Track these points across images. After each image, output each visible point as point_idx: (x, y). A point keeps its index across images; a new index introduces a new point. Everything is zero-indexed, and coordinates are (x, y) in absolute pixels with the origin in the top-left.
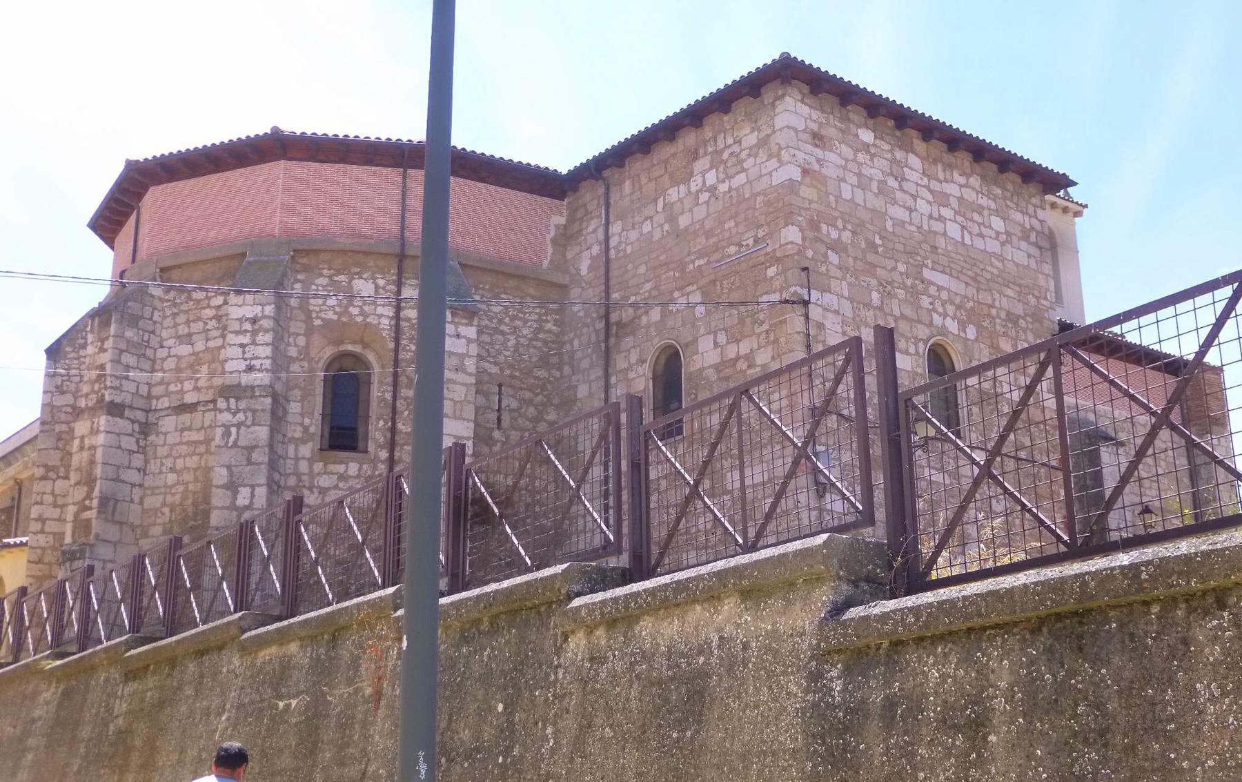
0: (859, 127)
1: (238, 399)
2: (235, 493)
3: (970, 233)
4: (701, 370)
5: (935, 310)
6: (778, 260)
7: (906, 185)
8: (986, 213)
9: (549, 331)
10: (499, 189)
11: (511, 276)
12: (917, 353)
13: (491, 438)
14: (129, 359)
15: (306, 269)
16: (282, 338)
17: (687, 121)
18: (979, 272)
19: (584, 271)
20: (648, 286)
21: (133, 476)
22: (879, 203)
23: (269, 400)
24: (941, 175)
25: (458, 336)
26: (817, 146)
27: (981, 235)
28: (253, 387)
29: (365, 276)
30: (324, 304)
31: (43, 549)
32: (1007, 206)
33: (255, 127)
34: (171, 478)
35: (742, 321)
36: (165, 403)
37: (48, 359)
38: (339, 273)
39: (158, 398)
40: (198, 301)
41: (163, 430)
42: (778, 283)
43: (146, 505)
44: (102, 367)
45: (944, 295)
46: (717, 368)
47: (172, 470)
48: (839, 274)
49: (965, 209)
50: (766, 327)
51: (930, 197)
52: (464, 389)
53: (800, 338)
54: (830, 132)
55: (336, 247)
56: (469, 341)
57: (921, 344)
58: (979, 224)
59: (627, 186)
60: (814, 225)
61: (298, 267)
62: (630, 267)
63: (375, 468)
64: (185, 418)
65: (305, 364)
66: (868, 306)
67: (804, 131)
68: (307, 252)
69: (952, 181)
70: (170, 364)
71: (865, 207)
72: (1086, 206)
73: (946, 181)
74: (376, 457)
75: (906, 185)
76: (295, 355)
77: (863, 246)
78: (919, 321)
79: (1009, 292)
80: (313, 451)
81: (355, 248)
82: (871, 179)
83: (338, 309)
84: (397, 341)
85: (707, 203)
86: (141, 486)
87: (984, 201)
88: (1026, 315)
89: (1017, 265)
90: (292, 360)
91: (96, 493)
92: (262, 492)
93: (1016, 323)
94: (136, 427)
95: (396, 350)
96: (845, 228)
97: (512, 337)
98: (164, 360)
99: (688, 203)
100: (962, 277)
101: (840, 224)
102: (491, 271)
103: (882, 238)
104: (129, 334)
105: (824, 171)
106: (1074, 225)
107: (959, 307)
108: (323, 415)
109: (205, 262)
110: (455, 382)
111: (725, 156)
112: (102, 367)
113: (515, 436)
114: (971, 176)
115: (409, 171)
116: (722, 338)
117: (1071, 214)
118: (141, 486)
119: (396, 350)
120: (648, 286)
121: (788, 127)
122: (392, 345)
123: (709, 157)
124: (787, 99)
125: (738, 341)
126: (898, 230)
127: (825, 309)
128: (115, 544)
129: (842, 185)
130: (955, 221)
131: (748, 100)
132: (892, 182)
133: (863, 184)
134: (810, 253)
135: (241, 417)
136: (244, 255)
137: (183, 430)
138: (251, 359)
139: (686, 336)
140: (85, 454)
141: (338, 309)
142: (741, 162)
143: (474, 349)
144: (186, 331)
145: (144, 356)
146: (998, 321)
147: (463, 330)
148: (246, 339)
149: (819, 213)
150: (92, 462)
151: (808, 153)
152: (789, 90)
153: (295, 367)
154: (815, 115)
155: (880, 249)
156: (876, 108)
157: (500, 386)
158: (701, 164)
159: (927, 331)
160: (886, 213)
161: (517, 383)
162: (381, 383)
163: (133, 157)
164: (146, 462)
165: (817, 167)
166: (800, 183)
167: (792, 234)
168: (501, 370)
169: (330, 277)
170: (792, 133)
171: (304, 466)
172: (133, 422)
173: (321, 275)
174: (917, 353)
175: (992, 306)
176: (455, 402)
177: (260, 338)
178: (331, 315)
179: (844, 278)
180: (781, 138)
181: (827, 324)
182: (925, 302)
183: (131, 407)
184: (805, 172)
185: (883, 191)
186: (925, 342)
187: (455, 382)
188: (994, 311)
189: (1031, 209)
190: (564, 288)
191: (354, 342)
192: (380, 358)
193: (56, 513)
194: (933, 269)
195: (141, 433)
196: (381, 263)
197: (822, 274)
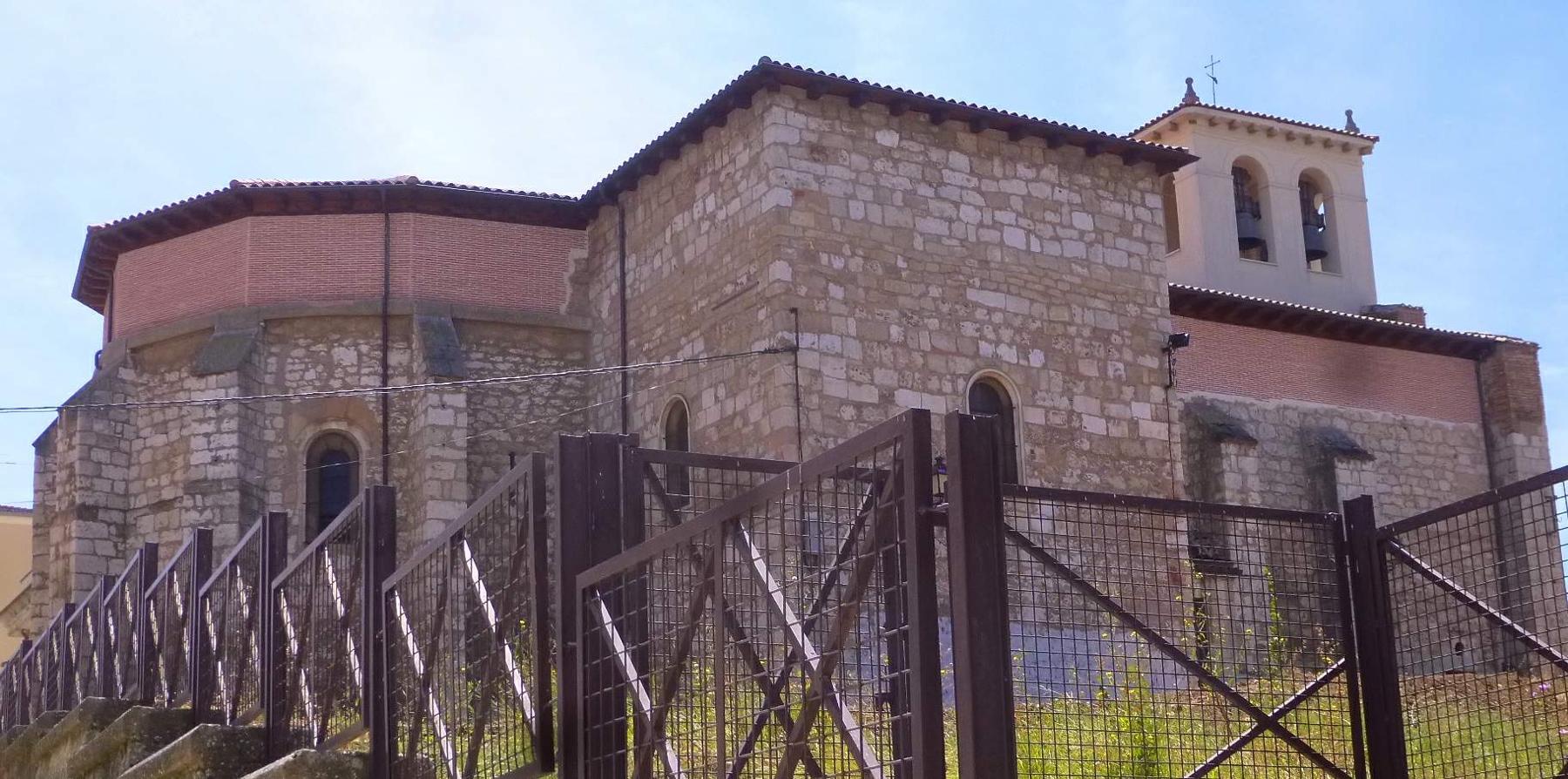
0: (876, 129)
1: (204, 495)
3: (1039, 237)
4: (705, 428)
5: (982, 338)
6: (768, 301)
7: (944, 192)
8: (1065, 210)
9: (571, 386)
10: (503, 224)
11: (518, 326)
12: (955, 392)
14: (100, 455)
15: (281, 340)
16: (254, 423)
17: (683, 139)
18: (1052, 283)
19: (605, 314)
20: (659, 331)
22: (904, 218)
23: (236, 495)
24: (998, 172)
25: (443, 406)
26: (815, 160)
27: (1057, 239)
28: (219, 481)
29: (346, 342)
30: (302, 378)
32: (1099, 197)
33: (214, 182)
35: (738, 371)
36: (143, 501)
37: (37, 453)
38: (316, 341)
39: (136, 496)
40: (173, 383)
41: (142, 531)
42: (768, 329)
45: (998, 318)
46: (718, 426)
48: (843, 309)
49: (1032, 208)
50: (757, 379)
51: (980, 201)
53: (789, 391)
54: (835, 141)
55: (310, 312)
56: (457, 410)
57: (961, 382)
58: (1054, 225)
59: (640, 212)
60: (810, 256)
61: (271, 339)
62: (644, 309)
64: (163, 516)
65: (284, 448)
66: (885, 342)
67: (799, 145)
68: (281, 321)
69: (1015, 177)
70: (146, 457)
71: (883, 225)
72: (1376, 139)
73: (1005, 177)
75: (944, 192)
76: (272, 439)
77: (880, 271)
78: (958, 353)
79: (1098, 303)
81: (332, 312)
82: (893, 191)
83: (317, 384)
85: (708, 233)
87: (1062, 195)
88: (1122, 329)
90: (270, 445)
93: (1106, 341)
94: (113, 529)
95: (385, 425)
96: (854, 254)
97: (525, 398)
98: (139, 452)
99: (691, 234)
100: (1024, 293)
101: (847, 250)
102: (495, 323)
103: (907, 260)
104: (99, 426)
105: (826, 189)
106: (1360, 164)
107: (1018, 331)
108: (308, 504)
109: (175, 339)
111: (722, 177)
112: (71, 466)
114: (1043, 166)
115: (394, 216)
116: (722, 392)
117: (1355, 152)
119: (385, 425)
120: (659, 331)
121: (776, 144)
122: (380, 419)
123: (708, 180)
124: (775, 109)
125: (735, 395)
126: (931, 247)
127: (822, 354)
129: (851, 203)
130: (1018, 226)
131: (737, 112)
132: (924, 190)
133: (881, 197)
134: (803, 291)
136: (212, 329)
138: (217, 449)
139: (692, 392)
140: (61, 563)
141: (317, 384)
142: (735, 185)
143: (463, 420)
144: (162, 418)
145: (118, 449)
146: (1078, 340)
148: (209, 428)
149: (816, 240)
150: (67, 572)
151: (804, 171)
152: (777, 98)
153: (273, 453)
154: (813, 124)
155: (904, 274)
156: (900, 105)
157: (512, 455)
158: (702, 187)
159: (970, 364)
160: (914, 229)
162: (370, 463)
165: (814, 186)
166: (790, 209)
167: (780, 270)
168: (513, 437)
169: (307, 347)
170: (781, 150)
172: (109, 525)
173: (297, 346)
174: (955, 392)
175: (1070, 324)
176: (443, 482)
177: (225, 426)
179: (852, 314)
180: (768, 157)
181: (826, 370)
182: (969, 329)
183: (107, 508)
184: (798, 194)
186: (967, 378)
188: (1072, 330)
189: (1136, 196)
190: (586, 334)
191: (338, 419)
192: (368, 435)
194: (982, 288)
195: (117, 536)
196: (364, 325)
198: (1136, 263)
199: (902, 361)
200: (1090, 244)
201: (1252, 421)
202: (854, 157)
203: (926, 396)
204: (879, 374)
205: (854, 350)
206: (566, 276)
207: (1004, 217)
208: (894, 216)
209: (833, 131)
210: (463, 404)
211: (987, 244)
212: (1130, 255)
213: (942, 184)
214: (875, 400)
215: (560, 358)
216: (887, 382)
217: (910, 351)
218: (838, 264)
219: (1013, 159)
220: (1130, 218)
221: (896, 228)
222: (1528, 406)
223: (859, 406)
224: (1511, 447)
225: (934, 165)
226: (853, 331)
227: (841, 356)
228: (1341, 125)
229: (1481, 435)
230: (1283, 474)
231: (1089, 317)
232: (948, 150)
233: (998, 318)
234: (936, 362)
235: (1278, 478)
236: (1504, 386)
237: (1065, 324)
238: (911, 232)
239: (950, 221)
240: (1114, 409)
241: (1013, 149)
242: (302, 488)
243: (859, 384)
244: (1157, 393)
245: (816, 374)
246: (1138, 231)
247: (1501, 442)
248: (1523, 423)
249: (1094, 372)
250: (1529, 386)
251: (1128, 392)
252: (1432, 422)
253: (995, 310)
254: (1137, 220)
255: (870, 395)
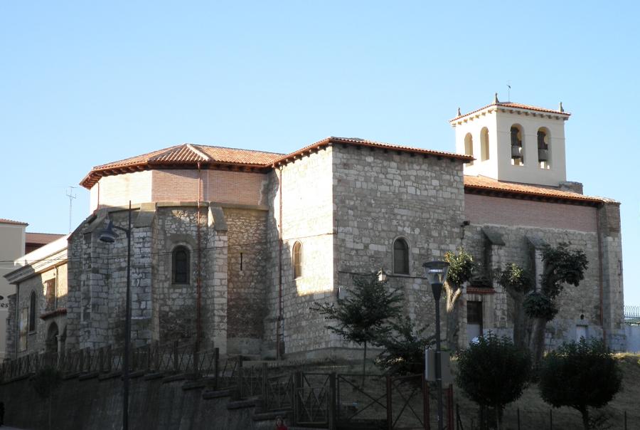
0: (366, 156)
2: (140, 303)
7: (388, 176)
8: (430, 179)
12: (389, 244)
13: (238, 275)
21: (104, 295)
24: (407, 167)
26: (345, 169)
27: (426, 189)
31: (73, 319)
32: (442, 174)
34: (118, 295)
43: (109, 306)
44: (90, 254)
45: (404, 218)
47: (118, 292)
51: (400, 178)
52: (222, 261)
56: (224, 242)
63: (193, 290)
66: (366, 229)
69: (413, 169)
73: (409, 169)
74: (193, 285)
77: (366, 205)
80: (169, 285)
82: (371, 177)
84: (199, 241)
86: (107, 298)
87: (429, 174)
88: (447, 219)
89: (444, 198)
91: (91, 303)
92: (149, 303)
96: (357, 199)
98: (113, 249)
106: (563, 124)
107: (411, 222)
110: (219, 258)
112: (90, 254)
113: (248, 273)
118: (107, 298)
122: (197, 242)
128: (99, 321)
129: (357, 182)
132: (381, 176)
134: (340, 213)
135: (141, 275)
137: (121, 277)
140: (86, 287)
147: (222, 238)
157: (241, 254)
161: (248, 252)
162: (194, 257)
163: (88, 190)
164: (109, 289)
165: (345, 177)
168: (242, 248)
171: (166, 291)
173: (169, 216)
175: (430, 218)
177: (146, 245)
178: (173, 232)
179: (356, 220)
181: (347, 239)
183: (101, 268)
185: (377, 180)
187: (219, 258)
191: (183, 241)
193: (76, 305)
194: (400, 208)
197: (345, 220)
198: (454, 196)
199: (372, 234)
200: (437, 191)
201: (506, 234)
202: (358, 167)
203: (379, 246)
204: (364, 239)
205: (356, 232)
206: (260, 191)
207: (408, 183)
208: (371, 186)
209: (351, 159)
210: (226, 240)
211: (402, 193)
212: (452, 193)
213: (387, 173)
214: (363, 248)
215: (258, 220)
216: (367, 242)
217: (374, 231)
218: (352, 203)
219: (412, 163)
220: (452, 180)
221: (372, 189)
222: (614, 227)
223: (357, 250)
224: (606, 242)
225: (385, 167)
226: (356, 226)
227: (352, 234)
228: (559, 111)
229: (597, 236)
230: (517, 253)
231: (436, 215)
232: (390, 161)
233: (404, 218)
234: (383, 234)
235: (515, 255)
236: (605, 219)
237: (428, 219)
238: (377, 190)
239: (390, 185)
240: (443, 247)
241: (413, 159)
242: (171, 264)
243: (357, 243)
244: (459, 240)
245: (343, 240)
246: (455, 184)
247: (603, 240)
248: (612, 233)
249: (436, 235)
250: (616, 218)
251: (448, 241)
252: (577, 232)
253: (404, 215)
254: (455, 181)
255: (360, 246)
